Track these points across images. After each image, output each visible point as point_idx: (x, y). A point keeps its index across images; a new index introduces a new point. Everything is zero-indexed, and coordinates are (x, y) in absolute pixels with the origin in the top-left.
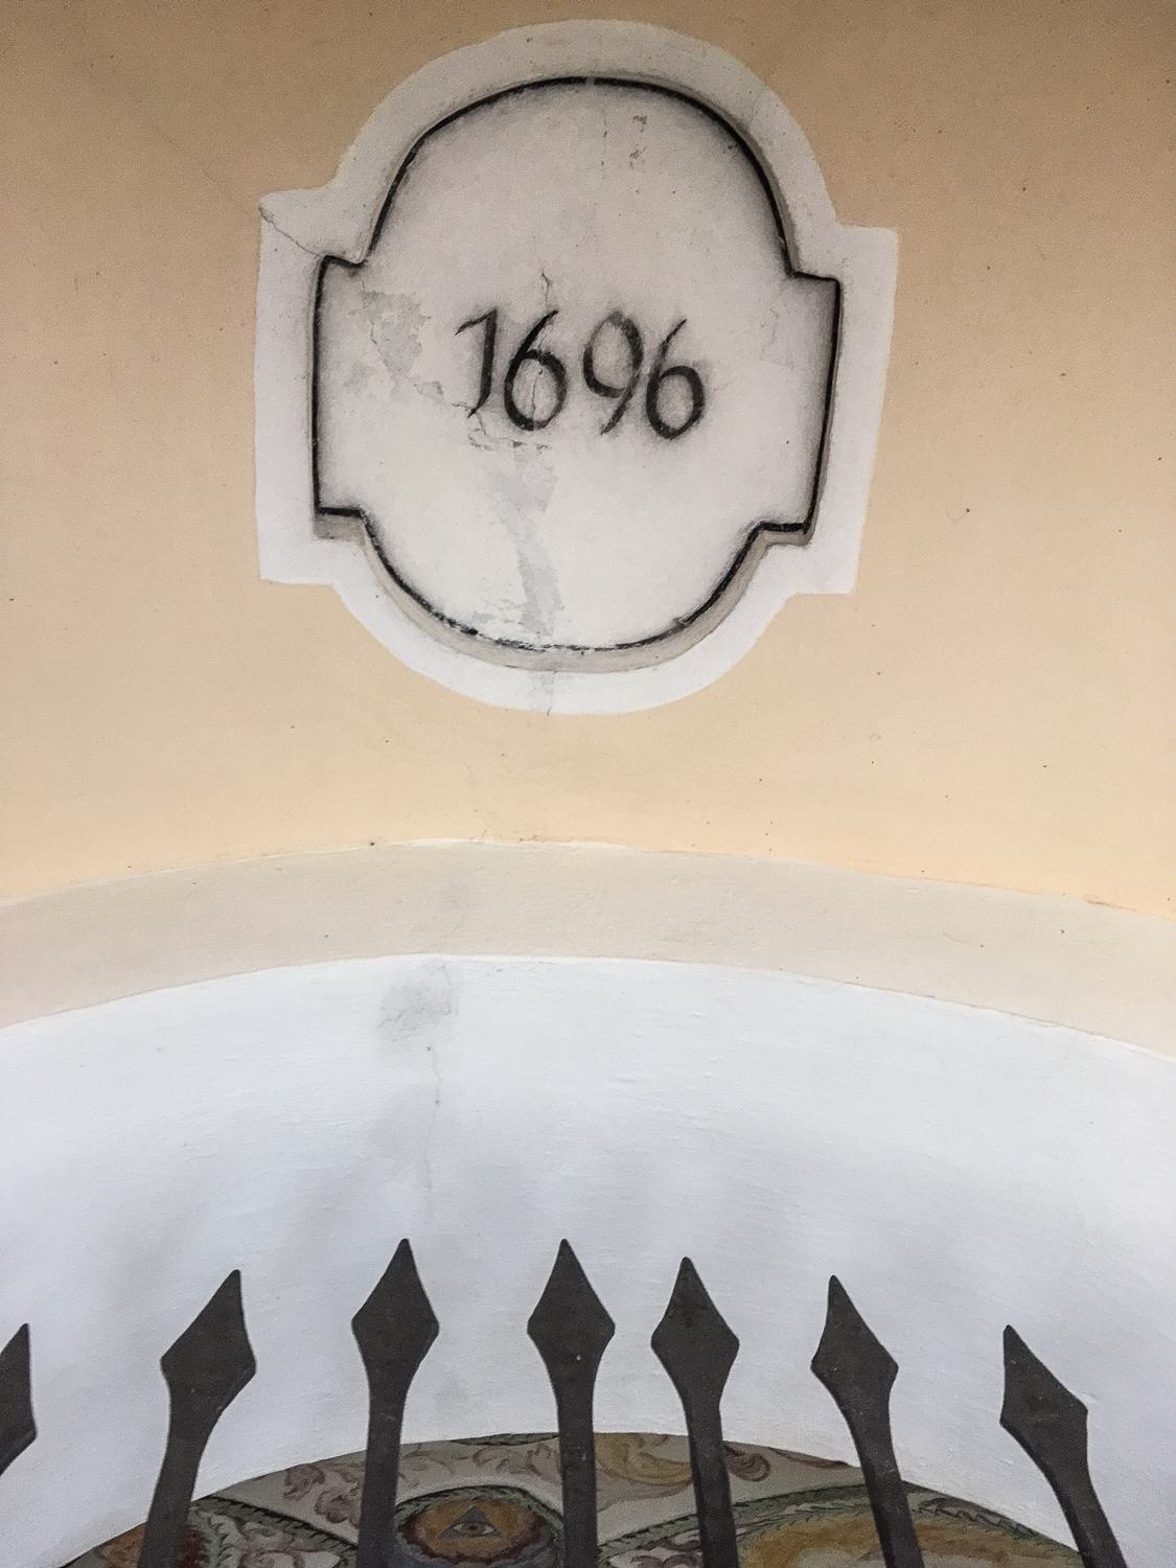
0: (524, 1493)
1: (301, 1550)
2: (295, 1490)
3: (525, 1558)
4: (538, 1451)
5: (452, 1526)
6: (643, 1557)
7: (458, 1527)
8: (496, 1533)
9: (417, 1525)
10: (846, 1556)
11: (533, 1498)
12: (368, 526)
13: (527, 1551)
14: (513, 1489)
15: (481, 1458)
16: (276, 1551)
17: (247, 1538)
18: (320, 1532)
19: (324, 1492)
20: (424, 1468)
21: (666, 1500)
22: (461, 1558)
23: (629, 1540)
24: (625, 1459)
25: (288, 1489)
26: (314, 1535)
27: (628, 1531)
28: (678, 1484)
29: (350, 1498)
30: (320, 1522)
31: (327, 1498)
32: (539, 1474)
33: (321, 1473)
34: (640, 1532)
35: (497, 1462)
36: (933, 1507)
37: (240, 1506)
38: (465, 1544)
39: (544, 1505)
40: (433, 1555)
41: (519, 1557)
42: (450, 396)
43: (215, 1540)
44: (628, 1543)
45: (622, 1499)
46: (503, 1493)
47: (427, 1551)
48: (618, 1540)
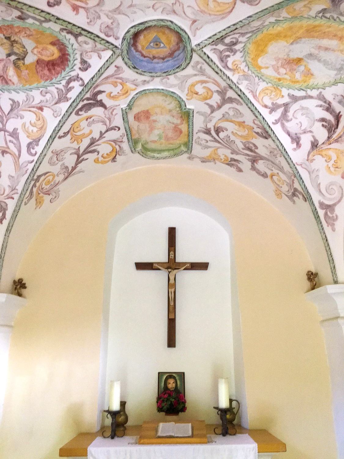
0: (172, 22)
1: (100, 51)
2: (91, 21)
3: (175, 57)
4: (175, 3)
5: (149, 44)
6: (215, 49)
7: (152, 44)
8: (164, 47)
9: (138, 44)
10: (285, 44)
11: (176, 25)
12: (4, 255)
13: (176, 53)
14: (167, 21)
15: (155, 7)
16: (91, 51)
17: (80, 46)
18: (103, 40)
19: (102, 24)
20: (135, 12)
21: (224, 20)
22: (154, 58)
23: (209, 39)
24: (208, 5)
25: (89, 21)
26: (101, 40)
27: (209, 36)
28: (226, 13)
29: (111, 27)
30: (102, 36)
31: (103, 26)
32: (177, 14)
33: (99, 15)
34: (213, 36)
35: (161, 9)
36: (321, 15)
37: (72, 25)
38: (155, 52)
39: (179, 27)
40: (145, 57)
41: (174, 57)
42: (319, 19)
43: (70, 47)
44: (209, 40)
45: (207, 23)
46: (164, 22)
47: (143, 55)
48: (206, 40)
